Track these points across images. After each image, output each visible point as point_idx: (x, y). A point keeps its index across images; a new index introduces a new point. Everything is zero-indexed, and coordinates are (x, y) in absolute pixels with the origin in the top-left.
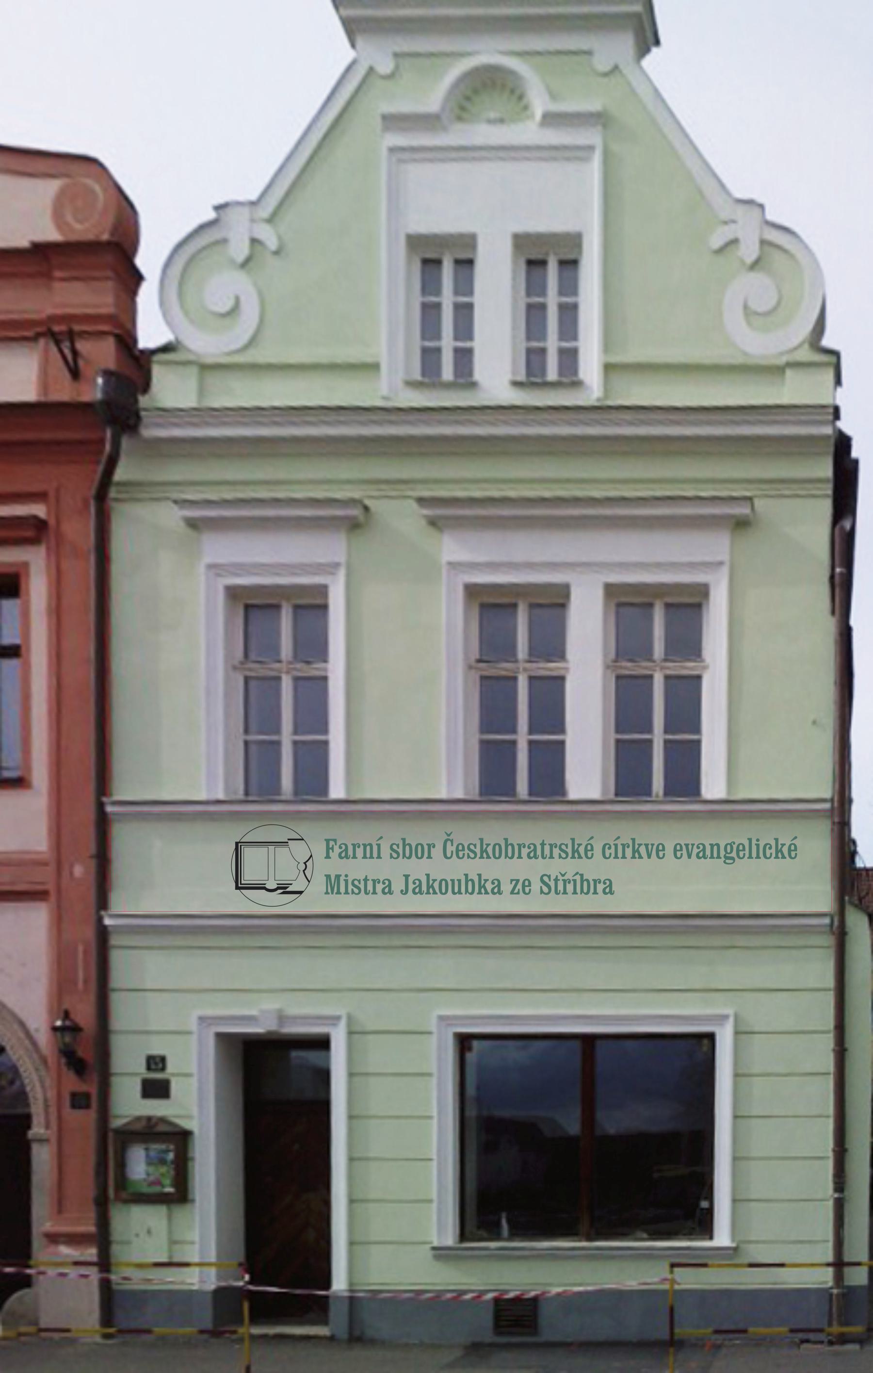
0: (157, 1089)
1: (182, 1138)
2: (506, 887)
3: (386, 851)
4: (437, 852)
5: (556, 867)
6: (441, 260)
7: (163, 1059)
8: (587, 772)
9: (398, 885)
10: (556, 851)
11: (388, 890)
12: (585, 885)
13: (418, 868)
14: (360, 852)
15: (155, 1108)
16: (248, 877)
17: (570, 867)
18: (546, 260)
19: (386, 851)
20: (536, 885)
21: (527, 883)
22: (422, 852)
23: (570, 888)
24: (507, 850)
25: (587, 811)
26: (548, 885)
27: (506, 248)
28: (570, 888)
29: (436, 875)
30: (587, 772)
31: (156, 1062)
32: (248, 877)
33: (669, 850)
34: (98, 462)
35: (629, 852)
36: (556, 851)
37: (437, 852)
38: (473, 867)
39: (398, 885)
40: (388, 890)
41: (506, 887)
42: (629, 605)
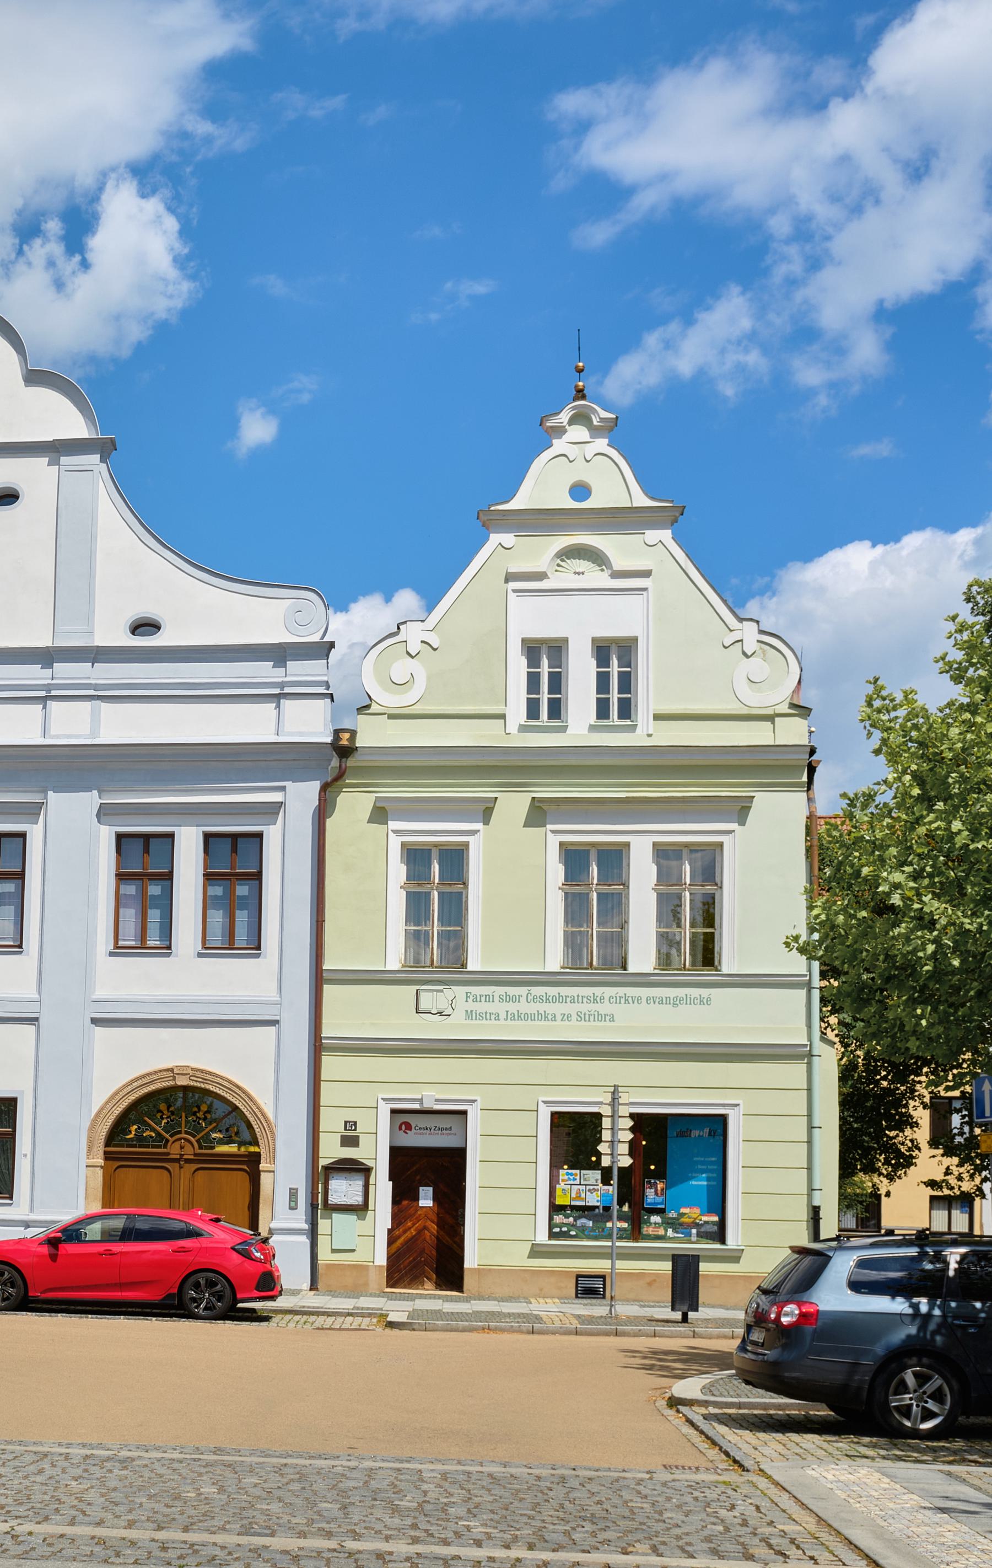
0: (350, 1141)
1: (366, 1171)
2: (559, 1017)
3: (497, 999)
4: (523, 999)
5: (585, 1008)
6: (545, 653)
7: (355, 1123)
8: (642, 954)
9: (502, 1016)
10: (585, 1000)
11: (497, 1018)
12: (600, 1017)
13: (512, 1007)
14: (483, 999)
15: (349, 1153)
16: (423, 1007)
17: (593, 1007)
18: (615, 653)
19: (497, 999)
20: (574, 1016)
21: (569, 1016)
22: (516, 999)
23: (592, 1018)
24: (559, 999)
25: (642, 980)
26: (516, 999)
27: (588, 648)
28: (592, 1018)
29: (522, 1011)
30: (642, 954)
31: (351, 1125)
32: (423, 1007)
33: (644, 1000)
34: (79, 381)
35: (623, 1000)
36: (585, 1000)
37: (523, 999)
38: (542, 1007)
39: (502, 1016)
40: (497, 1018)
41: (559, 1017)
42: (665, 855)
